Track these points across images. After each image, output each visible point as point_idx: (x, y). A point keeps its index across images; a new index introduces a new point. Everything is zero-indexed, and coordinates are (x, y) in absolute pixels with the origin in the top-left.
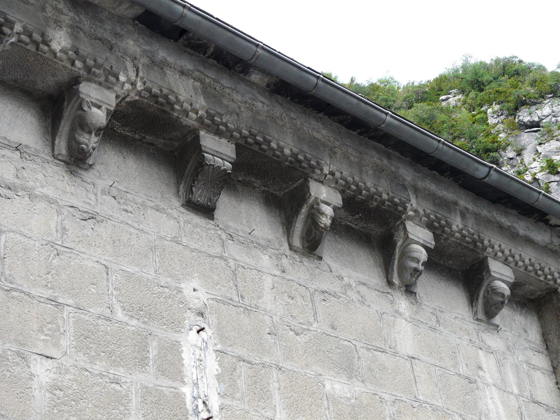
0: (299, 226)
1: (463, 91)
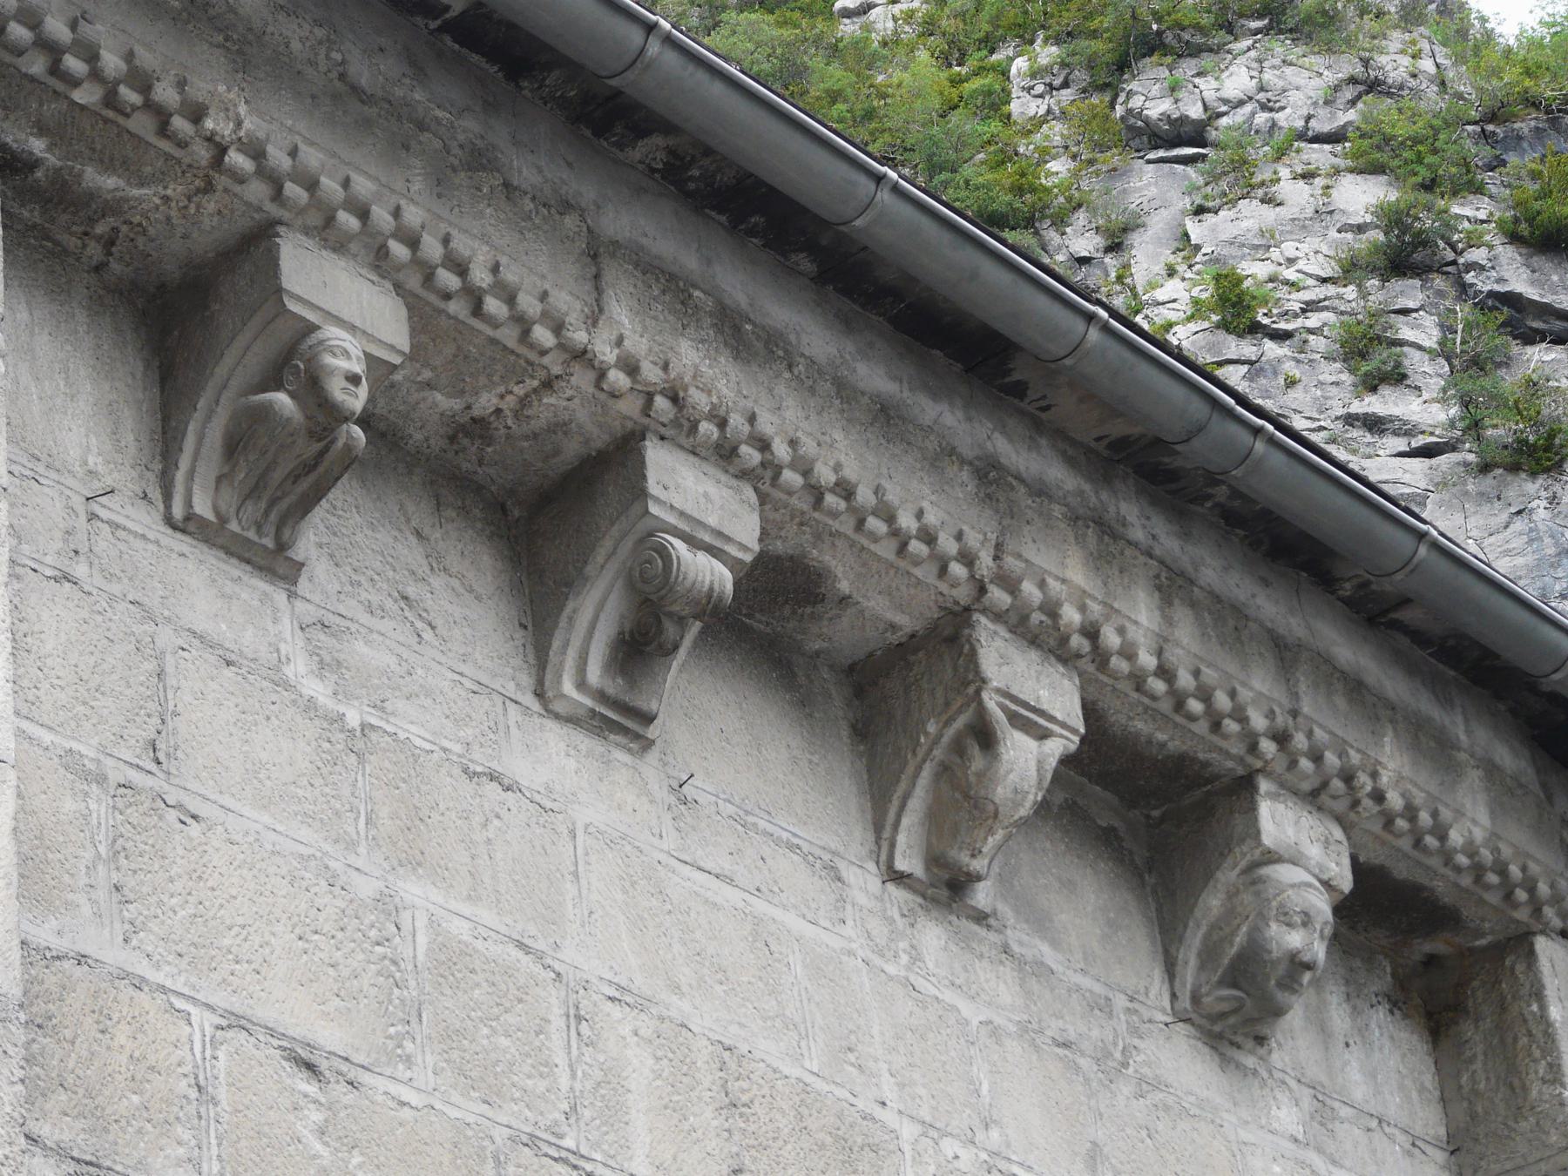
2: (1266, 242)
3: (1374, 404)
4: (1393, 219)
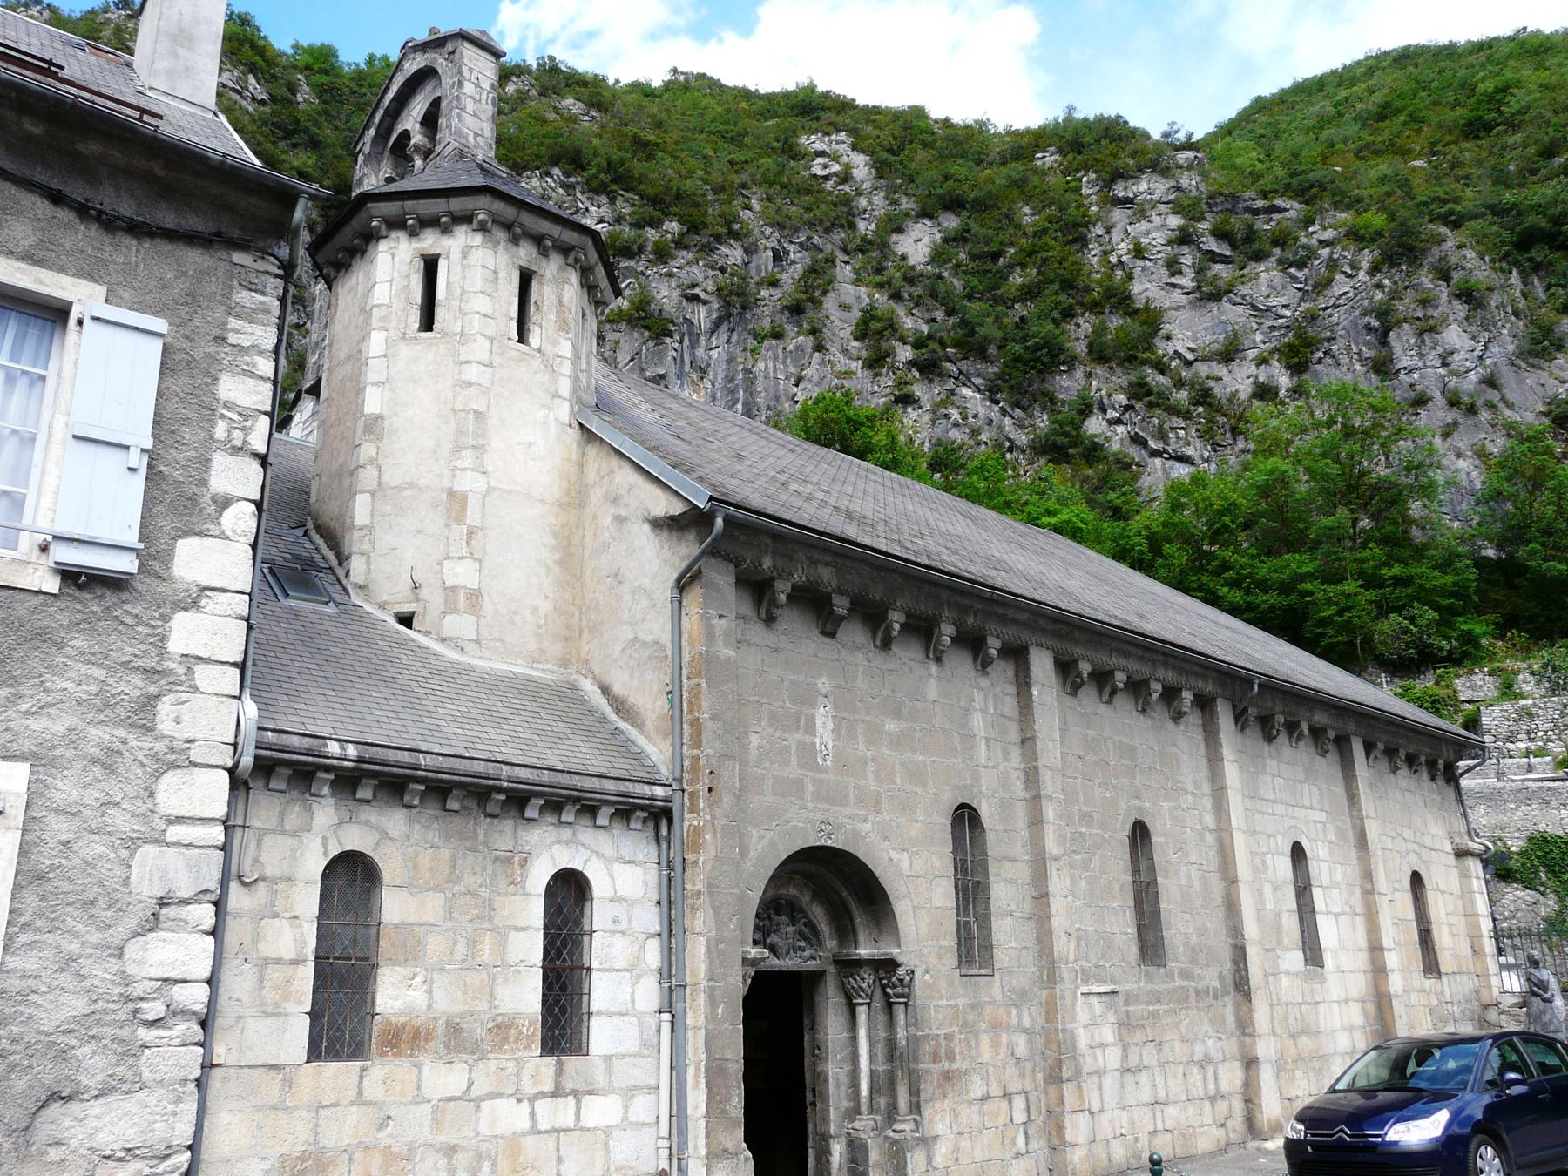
0: (880, 634)
1: (1060, 151)
2: (1148, 233)
3: (1173, 280)
4: (1181, 229)
